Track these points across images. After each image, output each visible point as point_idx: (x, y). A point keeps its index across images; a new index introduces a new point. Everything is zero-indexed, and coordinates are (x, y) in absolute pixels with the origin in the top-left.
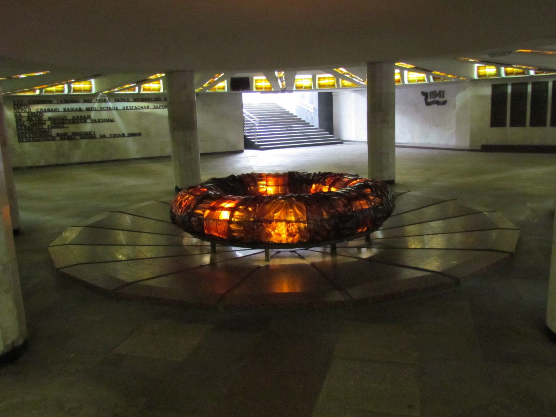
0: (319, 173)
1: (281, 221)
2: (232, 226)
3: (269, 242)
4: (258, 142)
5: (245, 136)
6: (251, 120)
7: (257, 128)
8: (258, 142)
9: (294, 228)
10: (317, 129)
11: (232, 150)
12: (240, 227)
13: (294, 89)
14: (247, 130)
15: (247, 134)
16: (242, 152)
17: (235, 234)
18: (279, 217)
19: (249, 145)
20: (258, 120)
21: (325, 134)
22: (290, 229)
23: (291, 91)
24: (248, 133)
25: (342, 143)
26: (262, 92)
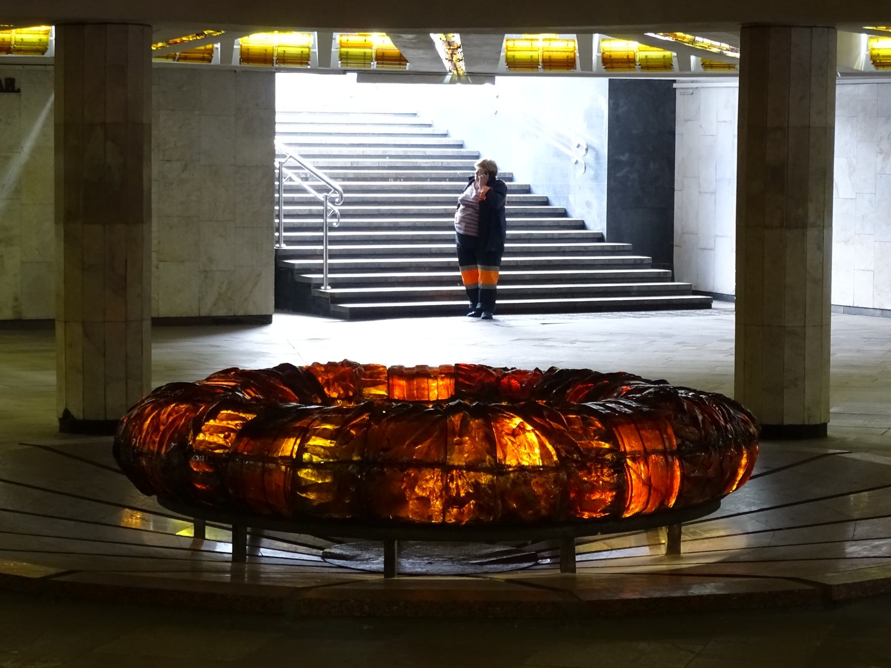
0: (552, 369)
1: (432, 465)
2: (303, 473)
3: (397, 519)
4: (335, 284)
5: (280, 256)
6: (305, 185)
7: (335, 222)
8: (335, 284)
9: (460, 485)
10: (599, 238)
11: (221, 312)
12: (324, 478)
13: (502, 65)
14: (288, 229)
15: (284, 247)
16: (265, 320)
17: (312, 496)
18: (427, 454)
19: (296, 294)
20: (337, 184)
21: (641, 267)
22: (453, 486)
23: (489, 77)
24: (289, 241)
25: (705, 305)
26: (366, 76)
